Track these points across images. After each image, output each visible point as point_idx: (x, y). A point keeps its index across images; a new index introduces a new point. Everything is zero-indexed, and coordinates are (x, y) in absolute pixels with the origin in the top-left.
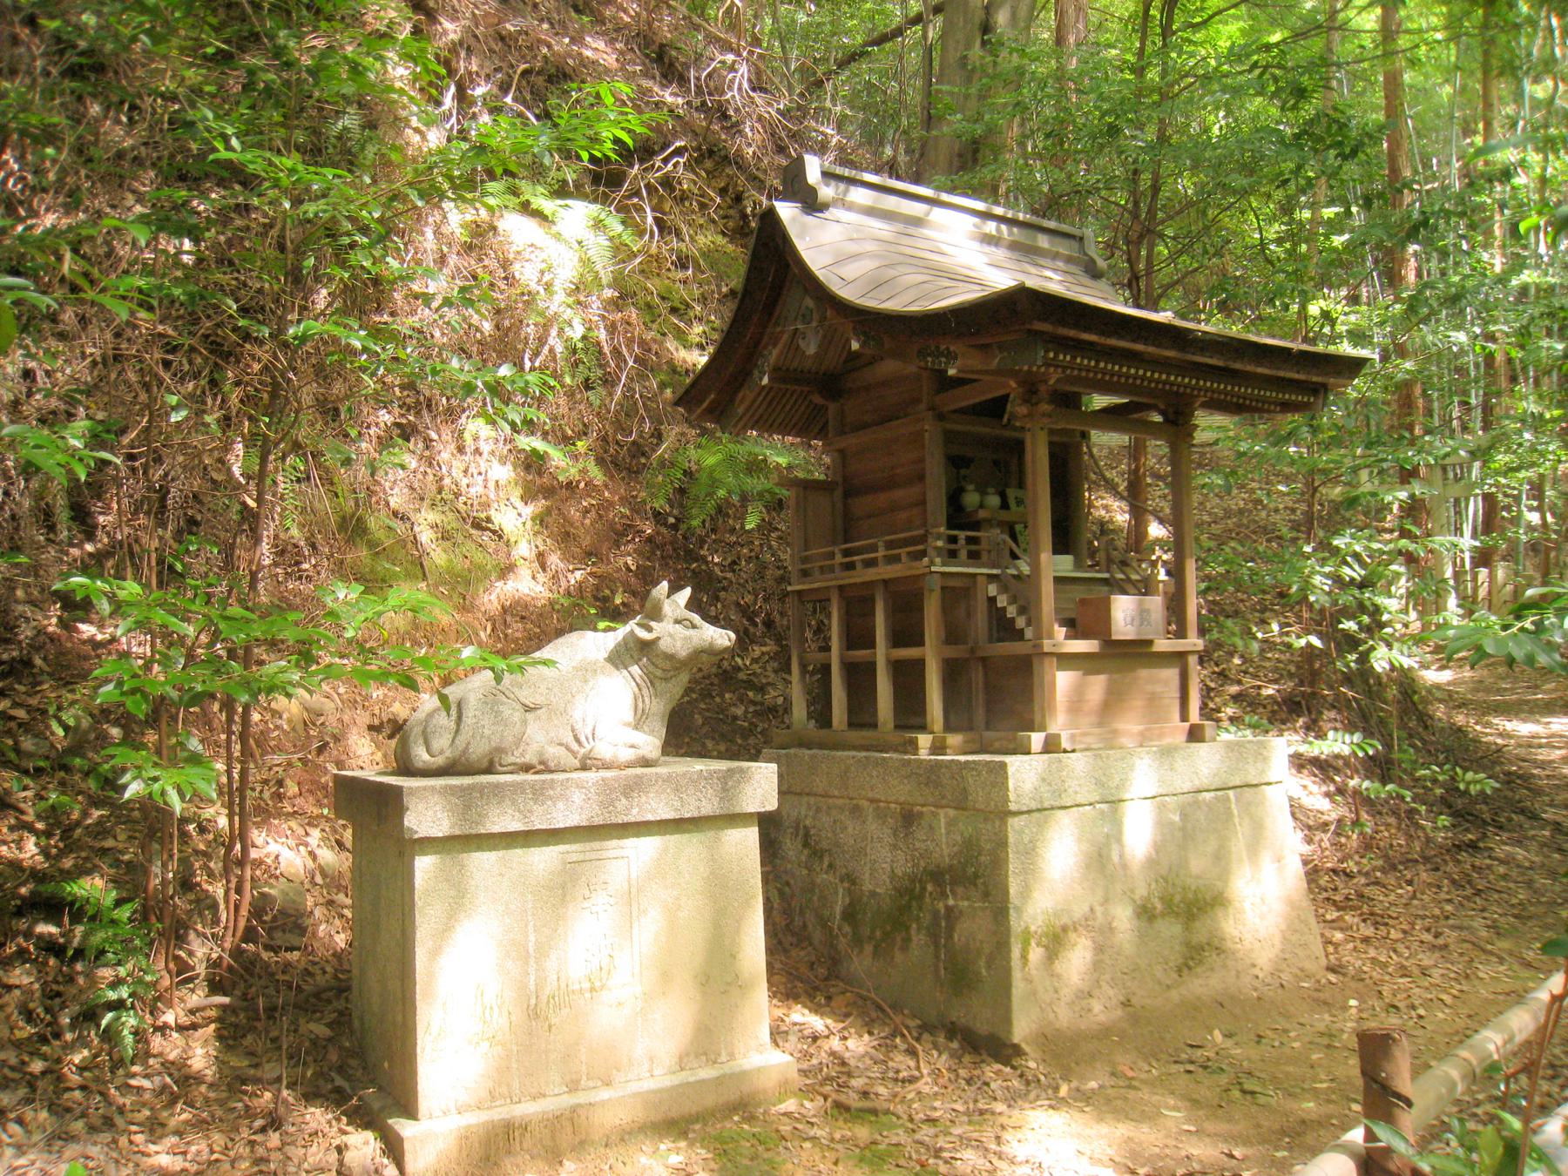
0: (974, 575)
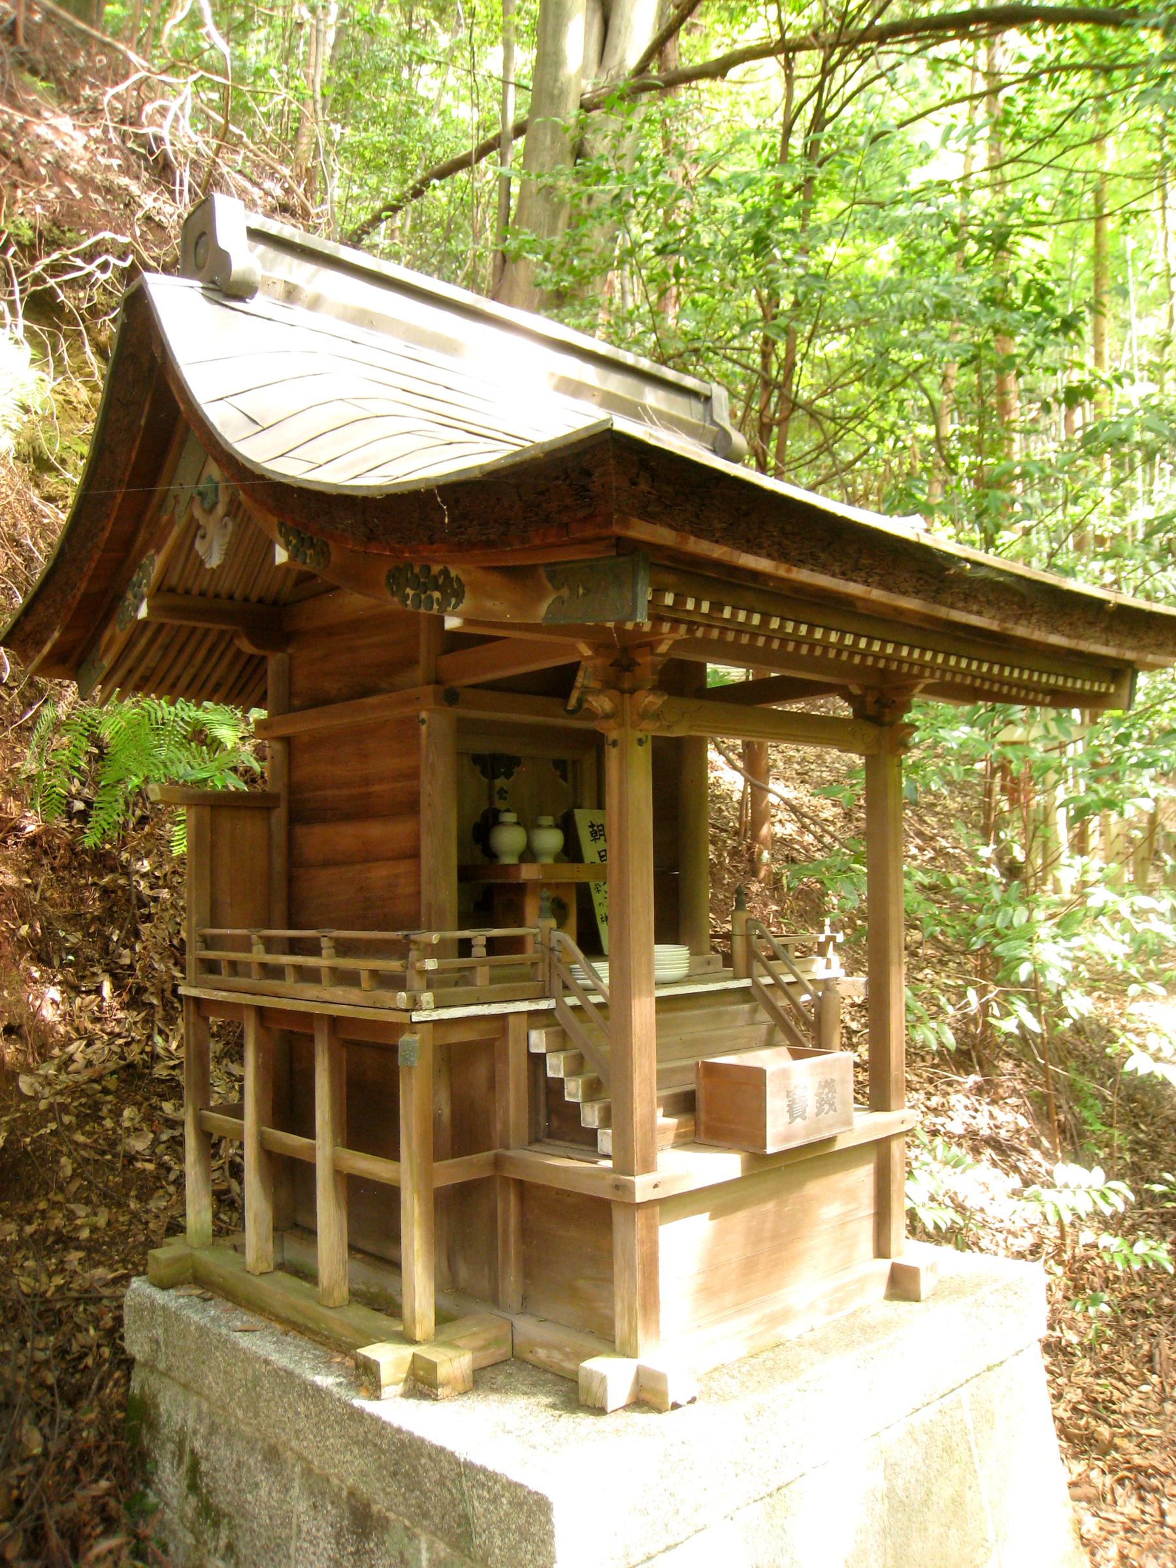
0: (504, 1017)
